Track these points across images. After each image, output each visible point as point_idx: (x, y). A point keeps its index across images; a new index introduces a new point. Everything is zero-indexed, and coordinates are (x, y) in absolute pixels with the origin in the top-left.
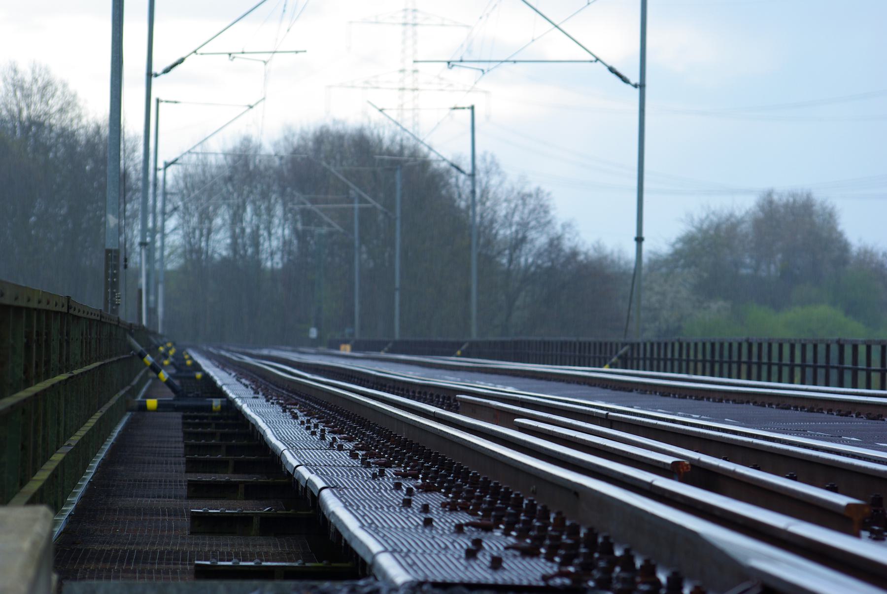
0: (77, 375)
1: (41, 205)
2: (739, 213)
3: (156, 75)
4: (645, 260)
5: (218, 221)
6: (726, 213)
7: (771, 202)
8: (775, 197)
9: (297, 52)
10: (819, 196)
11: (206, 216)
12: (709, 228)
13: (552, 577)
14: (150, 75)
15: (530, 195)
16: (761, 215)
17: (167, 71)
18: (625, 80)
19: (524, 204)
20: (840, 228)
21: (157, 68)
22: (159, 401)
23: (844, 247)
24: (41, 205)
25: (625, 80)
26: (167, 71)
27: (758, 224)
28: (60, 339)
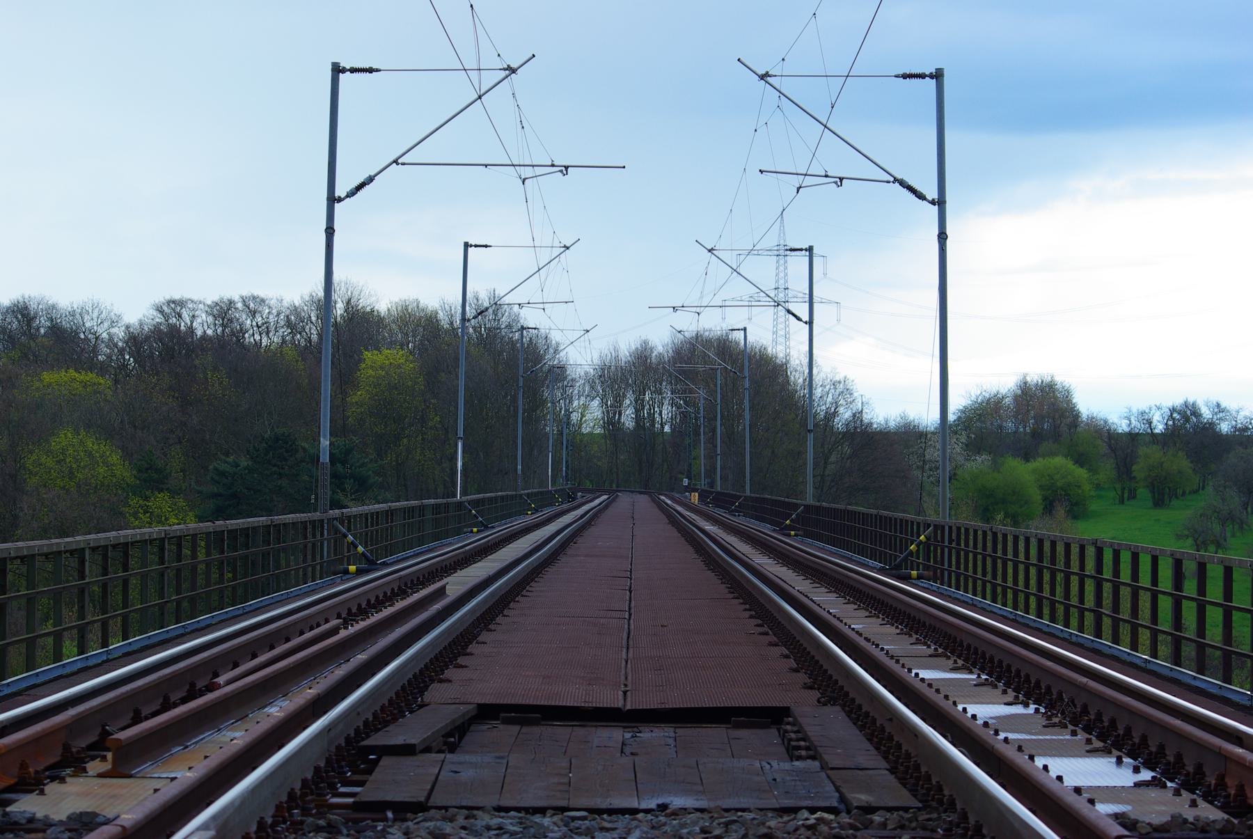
0: (113, 531)
1: (833, 484)
2: (1003, 391)
3: (340, 200)
4: (951, 417)
5: (628, 402)
6: (994, 391)
7: (1025, 383)
8: (1029, 379)
9: (486, 166)
10: (1059, 379)
11: (618, 401)
12: (983, 402)
13: (650, 359)
14: (332, 200)
15: (840, 382)
16: (1019, 392)
17: (351, 194)
18: (921, 197)
19: (835, 389)
20: (1074, 401)
21: (340, 191)
22: (357, 568)
23: (1077, 415)
24: (833, 484)
25: (921, 197)
26: (351, 194)
27: (1016, 398)
28: (231, 466)
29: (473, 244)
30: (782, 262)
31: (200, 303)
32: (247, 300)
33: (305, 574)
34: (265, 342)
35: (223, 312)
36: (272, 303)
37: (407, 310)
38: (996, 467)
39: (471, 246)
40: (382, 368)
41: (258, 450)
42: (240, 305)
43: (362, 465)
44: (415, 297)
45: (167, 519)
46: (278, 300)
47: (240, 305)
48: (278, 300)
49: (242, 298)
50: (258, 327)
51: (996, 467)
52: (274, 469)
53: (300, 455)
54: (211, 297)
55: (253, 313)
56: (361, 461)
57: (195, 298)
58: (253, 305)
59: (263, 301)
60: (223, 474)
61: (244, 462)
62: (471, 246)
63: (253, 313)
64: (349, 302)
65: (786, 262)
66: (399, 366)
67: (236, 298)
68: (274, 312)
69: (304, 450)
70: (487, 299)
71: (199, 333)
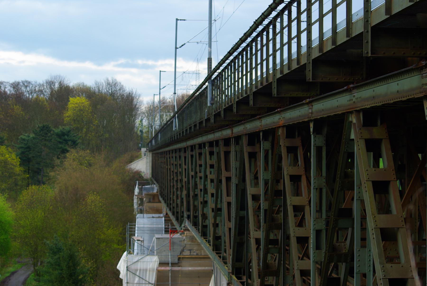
29: (179, 19)
30: (198, 76)
31: (8, 83)
32: (24, 82)
33: (251, 89)
34: (31, 97)
35: (15, 86)
36: (33, 83)
37: (80, 86)
38: (136, 196)
39: (179, 20)
40: (76, 104)
41: (37, 131)
42: (21, 84)
43: (74, 136)
44: (82, 82)
45: (5, 155)
46: (35, 82)
47: (21, 84)
48: (35, 82)
49: (22, 81)
50: (28, 92)
51: (136, 196)
52: (43, 137)
53: (52, 132)
54: (12, 81)
55: (26, 87)
56: (74, 135)
57: (6, 81)
58: (27, 84)
59: (29, 83)
60: (24, 140)
61: (32, 135)
62: (179, 20)
63: (26, 87)
64: (60, 83)
65: (199, 76)
66: (83, 103)
67: (20, 81)
68: (34, 86)
69: (53, 131)
70: (111, 80)
71: (9, 92)
